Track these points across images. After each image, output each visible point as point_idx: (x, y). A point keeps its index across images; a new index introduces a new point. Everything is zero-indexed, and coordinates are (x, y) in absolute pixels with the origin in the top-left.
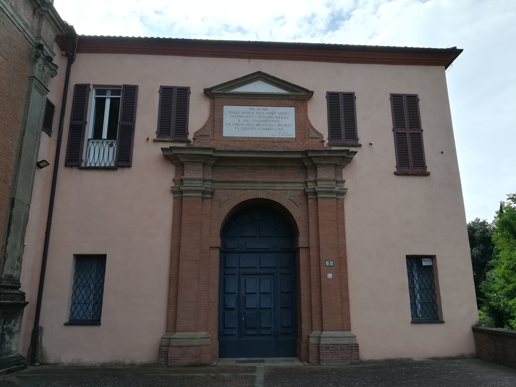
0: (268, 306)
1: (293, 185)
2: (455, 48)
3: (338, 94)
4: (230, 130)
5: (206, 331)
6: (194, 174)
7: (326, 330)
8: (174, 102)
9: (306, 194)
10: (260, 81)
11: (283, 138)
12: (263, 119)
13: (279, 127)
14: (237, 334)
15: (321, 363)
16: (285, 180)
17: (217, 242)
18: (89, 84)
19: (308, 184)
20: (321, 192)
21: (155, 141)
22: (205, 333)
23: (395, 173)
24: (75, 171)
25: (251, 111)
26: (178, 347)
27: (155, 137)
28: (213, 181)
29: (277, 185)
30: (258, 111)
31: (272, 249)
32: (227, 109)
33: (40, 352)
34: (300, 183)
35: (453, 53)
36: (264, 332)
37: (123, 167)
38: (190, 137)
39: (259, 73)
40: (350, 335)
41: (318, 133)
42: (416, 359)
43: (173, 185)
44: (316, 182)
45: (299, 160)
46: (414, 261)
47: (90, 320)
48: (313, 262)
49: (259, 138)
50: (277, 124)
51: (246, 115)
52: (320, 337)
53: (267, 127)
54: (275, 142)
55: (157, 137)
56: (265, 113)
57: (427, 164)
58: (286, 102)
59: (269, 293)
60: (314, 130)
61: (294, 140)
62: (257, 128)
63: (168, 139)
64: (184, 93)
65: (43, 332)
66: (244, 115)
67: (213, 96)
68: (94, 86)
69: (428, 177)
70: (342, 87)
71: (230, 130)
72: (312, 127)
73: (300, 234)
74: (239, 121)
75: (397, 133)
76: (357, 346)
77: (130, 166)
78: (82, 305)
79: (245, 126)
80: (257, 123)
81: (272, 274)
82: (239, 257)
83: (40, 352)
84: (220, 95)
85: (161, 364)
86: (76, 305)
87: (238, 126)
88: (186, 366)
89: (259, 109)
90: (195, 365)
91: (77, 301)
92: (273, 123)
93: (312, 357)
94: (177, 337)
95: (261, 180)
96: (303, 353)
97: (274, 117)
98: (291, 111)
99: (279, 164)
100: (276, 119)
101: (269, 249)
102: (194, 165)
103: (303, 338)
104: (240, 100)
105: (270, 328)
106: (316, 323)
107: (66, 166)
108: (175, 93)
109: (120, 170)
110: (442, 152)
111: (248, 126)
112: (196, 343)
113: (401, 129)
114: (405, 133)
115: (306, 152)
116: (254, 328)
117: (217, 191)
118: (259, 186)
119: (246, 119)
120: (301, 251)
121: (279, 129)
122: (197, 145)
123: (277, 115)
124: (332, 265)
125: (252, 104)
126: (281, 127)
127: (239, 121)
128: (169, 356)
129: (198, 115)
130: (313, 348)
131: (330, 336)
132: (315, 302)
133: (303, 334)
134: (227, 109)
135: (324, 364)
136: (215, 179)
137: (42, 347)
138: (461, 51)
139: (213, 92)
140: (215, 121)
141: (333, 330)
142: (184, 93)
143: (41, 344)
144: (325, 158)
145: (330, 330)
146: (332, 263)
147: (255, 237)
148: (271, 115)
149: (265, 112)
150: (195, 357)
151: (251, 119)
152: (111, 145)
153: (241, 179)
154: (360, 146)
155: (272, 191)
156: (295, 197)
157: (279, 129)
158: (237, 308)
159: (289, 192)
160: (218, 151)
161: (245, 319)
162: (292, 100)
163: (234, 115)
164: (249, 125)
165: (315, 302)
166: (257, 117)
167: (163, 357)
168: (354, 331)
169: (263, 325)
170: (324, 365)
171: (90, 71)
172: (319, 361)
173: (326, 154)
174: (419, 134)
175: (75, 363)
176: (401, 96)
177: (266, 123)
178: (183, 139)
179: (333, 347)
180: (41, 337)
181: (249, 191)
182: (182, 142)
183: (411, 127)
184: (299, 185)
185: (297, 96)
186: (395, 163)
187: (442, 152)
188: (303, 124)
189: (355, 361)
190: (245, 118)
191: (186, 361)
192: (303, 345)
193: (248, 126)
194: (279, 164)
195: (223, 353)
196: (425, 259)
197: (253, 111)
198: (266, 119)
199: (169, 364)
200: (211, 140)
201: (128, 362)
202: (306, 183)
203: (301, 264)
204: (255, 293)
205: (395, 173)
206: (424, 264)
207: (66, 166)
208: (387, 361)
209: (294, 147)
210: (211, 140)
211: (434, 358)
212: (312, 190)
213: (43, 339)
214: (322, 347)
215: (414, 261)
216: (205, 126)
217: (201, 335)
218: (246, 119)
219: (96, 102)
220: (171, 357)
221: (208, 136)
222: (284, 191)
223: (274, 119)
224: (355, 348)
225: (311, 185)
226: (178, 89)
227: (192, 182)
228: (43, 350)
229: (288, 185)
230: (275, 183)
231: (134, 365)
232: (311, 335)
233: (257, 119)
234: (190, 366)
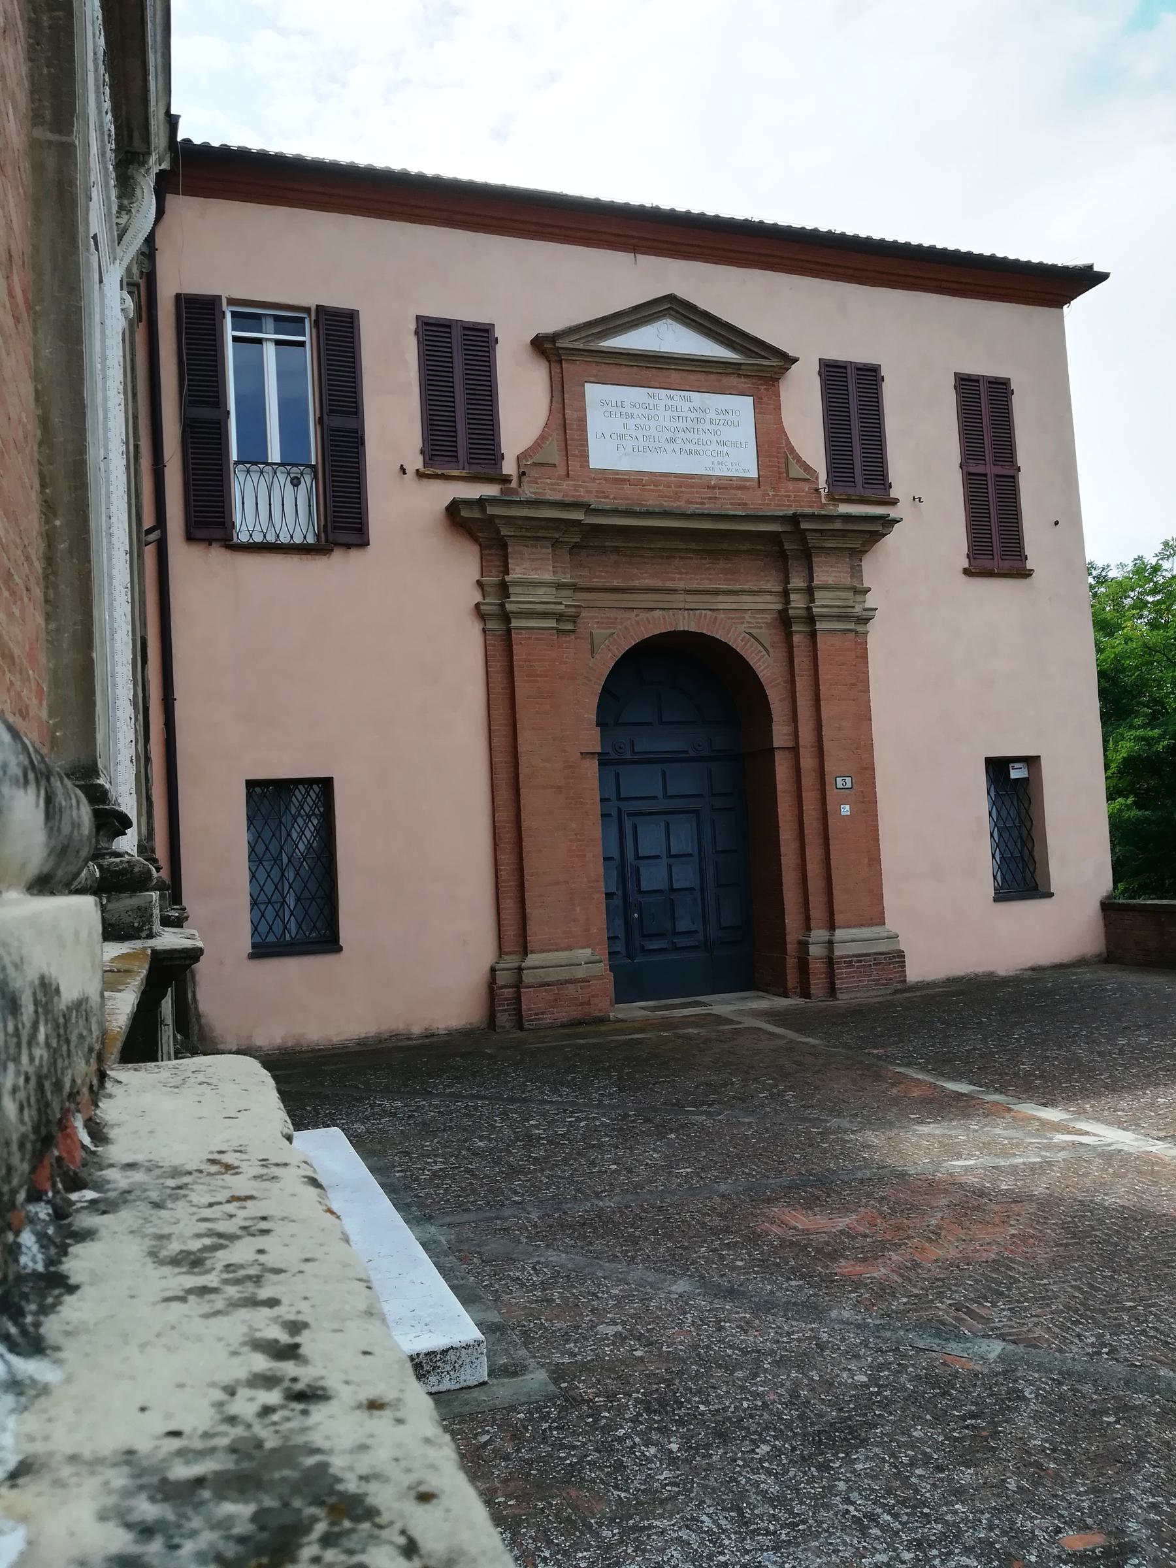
0: (688, 885)
1: (757, 599)
2: (1091, 267)
3: (449, 327)
4: (604, 454)
5: (588, 946)
6: (535, 572)
7: (839, 927)
8: (456, 359)
9: (784, 620)
10: (670, 321)
11: (730, 478)
12: (681, 425)
13: (720, 448)
14: (643, 946)
15: (839, 995)
16: (738, 587)
17: (592, 740)
18: (220, 297)
19: (793, 597)
20: (824, 616)
21: (420, 475)
22: (588, 951)
23: (966, 572)
24: (217, 556)
25: (652, 402)
26: (543, 985)
27: (416, 462)
28: (575, 588)
29: (720, 598)
30: (670, 403)
31: (692, 753)
32: (595, 393)
33: (196, 1028)
34: (770, 592)
35: (1084, 279)
36: (682, 942)
37: (348, 546)
38: (509, 467)
39: (671, 298)
40: (886, 934)
41: (807, 468)
42: (1002, 972)
43: (477, 597)
44: (810, 591)
45: (775, 537)
46: (997, 767)
47: (273, 945)
48: (809, 780)
49: (676, 476)
50: (714, 438)
51: (641, 411)
52: (520, 969)
53: (693, 447)
54: (714, 488)
55: (425, 465)
56: (686, 409)
57: (1029, 550)
58: (733, 381)
59: (690, 855)
60: (798, 459)
61: (755, 484)
62: (669, 447)
63: (456, 473)
64: (480, 337)
65: (198, 978)
66: (635, 411)
67: (559, 355)
68: (232, 302)
69: (1028, 580)
70: (853, 351)
71: (604, 454)
72: (792, 450)
73: (775, 719)
74: (625, 426)
75: (970, 474)
76: (901, 954)
77: (364, 544)
78: (263, 907)
79: (641, 443)
80: (669, 435)
81: (695, 812)
82: (617, 775)
83: (196, 1028)
84: (567, 354)
85: (503, 1027)
86: (263, 907)
87: (624, 442)
88: (563, 1026)
89: (671, 398)
90: (581, 1023)
91: (262, 898)
92: (705, 437)
93: (817, 984)
94: (537, 963)
95: (681, 585)
96: (792, 978)
97: (708, 421)
98: (744, 406)
99: (725, 546)
100: (712, 427)
101: (686, 752)
102: (532, 546)
103: (788, 946)
104: (625, 369)
105: (696, 932)
106: (818, 912)
107: (190, 538)
108: (457, 336)
109: (338, 556)
110: (1057, 523)
111: (646, 443)
112: (580, 973)
113: (977, 464)
114: (985, 475)
115: (795, 519)
116: (660, 935)
117: (585, 614)
118: (679, 600)
119: (643, 422)
120: (778, 756)
121: (720, 453)
122: (528, 492)
123: (712, 415)
124: (849, 785)
125: (653, 384)
126: (725, 449)
127: (625, 426)
128: (524, 1007)
129: (522, 406)
130: (817, 967)
131: (851, 940)
132: (814, 869)
133: (789, 938)
134: (595, 393)
135: (844, 996)
136: (581, 583)
137: (199, 1016)
138: (1103, 277)
139: (563, 343)
140: (566, 425)
141: (855, 926)
142: (480, 337)
143: (196, 1008)
144: (834, 533)
145: (849, 927)
146: (848, 780)
147: (650, 724)
148: (700, 415)
149: (686, 405)
150: (581, 1004)
151: (653, 423)
152: (296, 482)
153: (636, 583)
154: (894, 502)
155: (709, 613)
156: (761, 628)
157: (720, 453)
158: (620, 893)
159: (747, 616)
160: (594, 510)
161: (640, 916)
162: (746, 376)
163: (614, 409)
164: (648, 438)
165: (814, 869)
166: (667, 418)
167: (505, 1011)
168: (892, 923)
169: (682, 926)
170: (844, 998)
171: (227, 253)
172: (832, 991)
173: (838, 526)
174: (1013, 477)
175: (289, 1044)
176: (978, 381)
177: (690, 436)
178: (491, 472)
179: (860, 961)
180: (194, 993)
181: (657, 613)
182: (490, 480)
183: (996, 462)
184: (768, 598)
185: (756, 366)
186: (965, 549)
187: (1057, 523)
188: (773, 445)
189: (899, 986)
190: (638, 421)
191: (562, 1014)
192: (791, 962)
193: (646, 443)
194: (725, 546)
195: (623, 995)
196: (1016, 766)
197: (657, 401)
198: (689, 425)
199: (526, 1025)
200: (560, 478)
201: (417, 1030)
202: (785, 594)
203: (779, 787)
204: (658, 857)
205: (966, 572)
206: (1015, 774)
207: (190, 538)
208: (950, 981)
209: (759, 502)
210: (560, 478)
211: (1033, 969)
212: (803, 612)
213: (199, 996)
214: (838, 963)
215: (997, 767)
216: (543, 438)
217: (575, 956)
218: (643, 422)
219: (299, 353)
220: (529, 1010)
221: (554, 465)
222: (735, 612)
223: (707, 426)
224: (899, 957)
225: (798, 602)
226: (465, 328)
227: (532, 590)
228: (203, 1021)
229: (746, 598)
230: (717, 592)
231: (433, 1035)
232: (810, 940)
233: (667, 424)
234: (572, 1025)
